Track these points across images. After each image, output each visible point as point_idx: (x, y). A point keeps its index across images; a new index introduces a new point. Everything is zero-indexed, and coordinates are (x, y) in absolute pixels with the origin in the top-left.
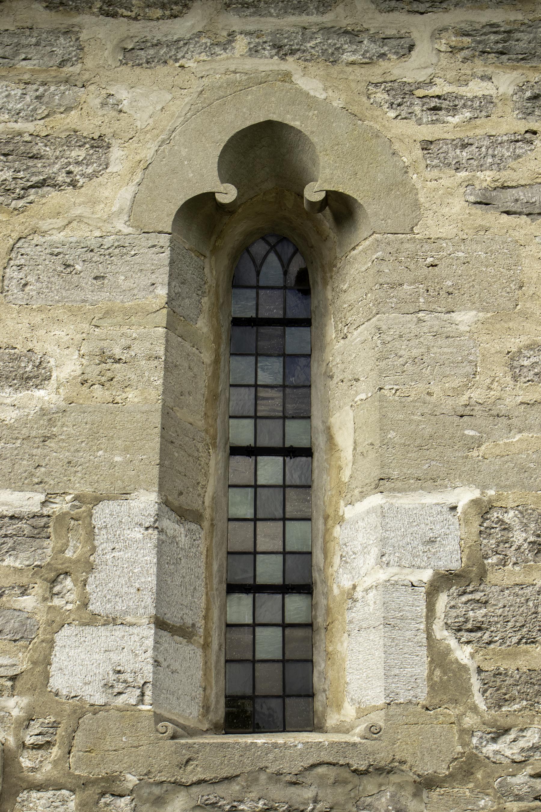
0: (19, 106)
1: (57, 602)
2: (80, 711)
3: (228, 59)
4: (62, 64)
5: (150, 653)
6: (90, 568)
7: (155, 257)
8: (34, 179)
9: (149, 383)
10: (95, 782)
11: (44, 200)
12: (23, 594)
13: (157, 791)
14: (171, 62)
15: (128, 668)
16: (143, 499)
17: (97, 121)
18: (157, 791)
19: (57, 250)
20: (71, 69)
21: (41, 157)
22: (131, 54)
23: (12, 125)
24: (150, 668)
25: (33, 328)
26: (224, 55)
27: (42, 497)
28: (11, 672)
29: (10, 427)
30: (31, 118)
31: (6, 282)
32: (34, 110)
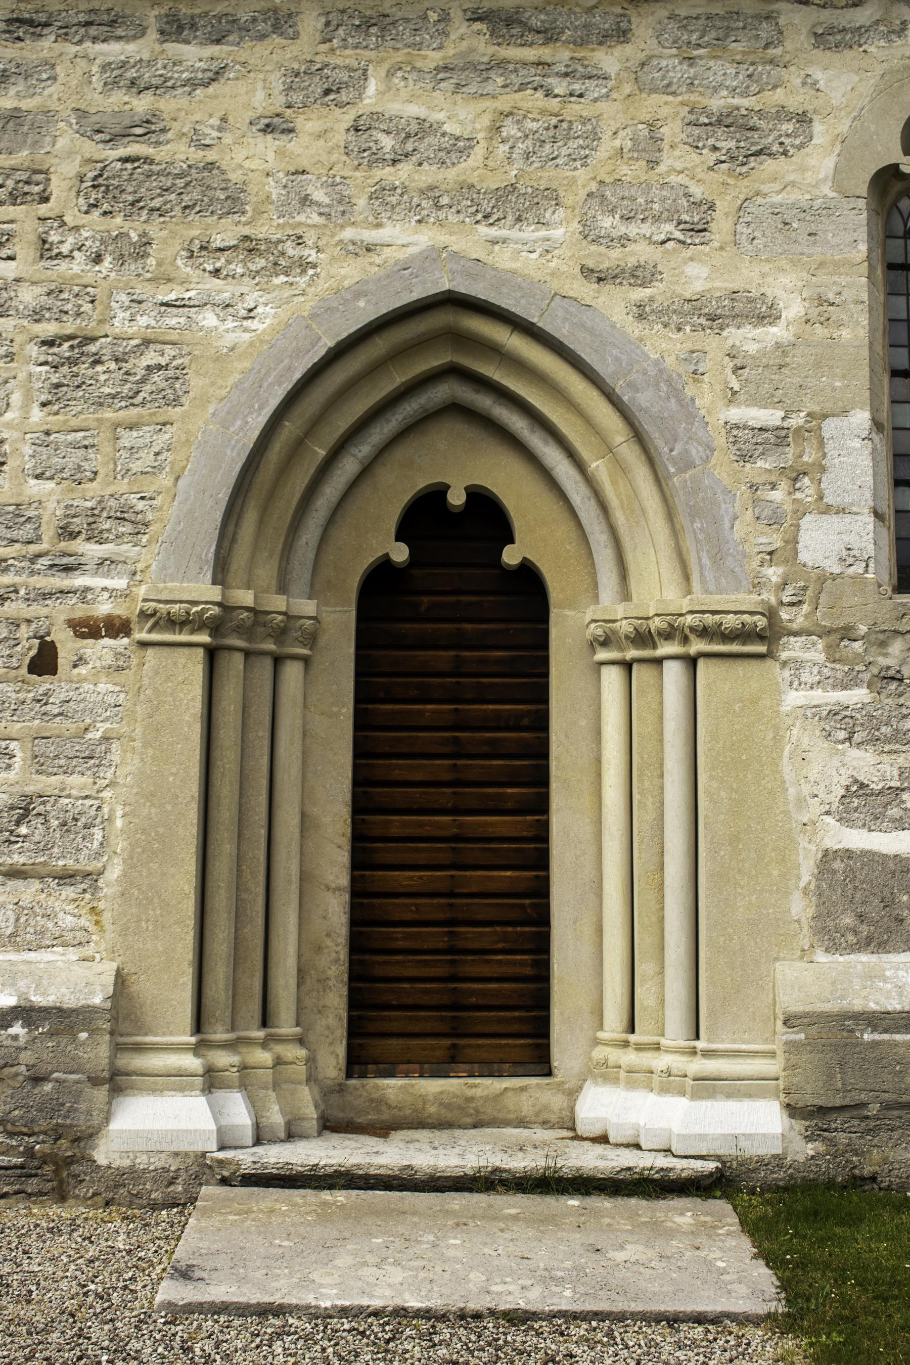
0: (735, 83)
1: (798, 495)
2: (823, 578)
3: (902, 45)
4: (767, 46)
5: (871, 535)
6: (823, 469)
7: (855, 218)
8: (754, 148)
9: (858, 323)
10: (836, 630)
11: (762, 167)
12: (772, 489)
13: (881, 637)
14: (856, 47)
15: (856, 546)
16: (859, 416)
17: (800, 99)
18: (881, 637)
19: (777, 211)
20: (774, 51)
21: (757, 129)
22: (823, 38)
23: (730, 100)
24: (872, 546)
25: (763, 276)
26: (899, 43)
27: (782, 414)
28: (769, 549)
29: (753, 357)
30: (745, 94)
31: (738, 237)
32: (748, 87)
